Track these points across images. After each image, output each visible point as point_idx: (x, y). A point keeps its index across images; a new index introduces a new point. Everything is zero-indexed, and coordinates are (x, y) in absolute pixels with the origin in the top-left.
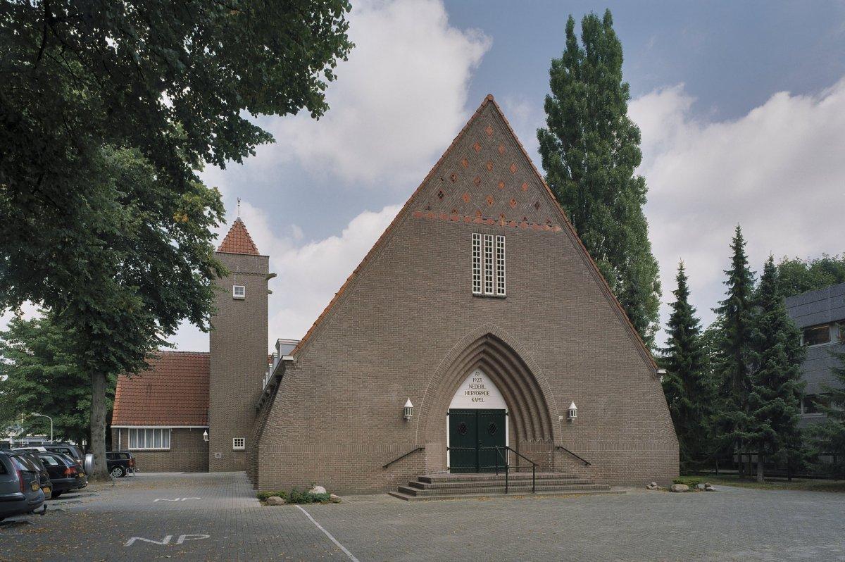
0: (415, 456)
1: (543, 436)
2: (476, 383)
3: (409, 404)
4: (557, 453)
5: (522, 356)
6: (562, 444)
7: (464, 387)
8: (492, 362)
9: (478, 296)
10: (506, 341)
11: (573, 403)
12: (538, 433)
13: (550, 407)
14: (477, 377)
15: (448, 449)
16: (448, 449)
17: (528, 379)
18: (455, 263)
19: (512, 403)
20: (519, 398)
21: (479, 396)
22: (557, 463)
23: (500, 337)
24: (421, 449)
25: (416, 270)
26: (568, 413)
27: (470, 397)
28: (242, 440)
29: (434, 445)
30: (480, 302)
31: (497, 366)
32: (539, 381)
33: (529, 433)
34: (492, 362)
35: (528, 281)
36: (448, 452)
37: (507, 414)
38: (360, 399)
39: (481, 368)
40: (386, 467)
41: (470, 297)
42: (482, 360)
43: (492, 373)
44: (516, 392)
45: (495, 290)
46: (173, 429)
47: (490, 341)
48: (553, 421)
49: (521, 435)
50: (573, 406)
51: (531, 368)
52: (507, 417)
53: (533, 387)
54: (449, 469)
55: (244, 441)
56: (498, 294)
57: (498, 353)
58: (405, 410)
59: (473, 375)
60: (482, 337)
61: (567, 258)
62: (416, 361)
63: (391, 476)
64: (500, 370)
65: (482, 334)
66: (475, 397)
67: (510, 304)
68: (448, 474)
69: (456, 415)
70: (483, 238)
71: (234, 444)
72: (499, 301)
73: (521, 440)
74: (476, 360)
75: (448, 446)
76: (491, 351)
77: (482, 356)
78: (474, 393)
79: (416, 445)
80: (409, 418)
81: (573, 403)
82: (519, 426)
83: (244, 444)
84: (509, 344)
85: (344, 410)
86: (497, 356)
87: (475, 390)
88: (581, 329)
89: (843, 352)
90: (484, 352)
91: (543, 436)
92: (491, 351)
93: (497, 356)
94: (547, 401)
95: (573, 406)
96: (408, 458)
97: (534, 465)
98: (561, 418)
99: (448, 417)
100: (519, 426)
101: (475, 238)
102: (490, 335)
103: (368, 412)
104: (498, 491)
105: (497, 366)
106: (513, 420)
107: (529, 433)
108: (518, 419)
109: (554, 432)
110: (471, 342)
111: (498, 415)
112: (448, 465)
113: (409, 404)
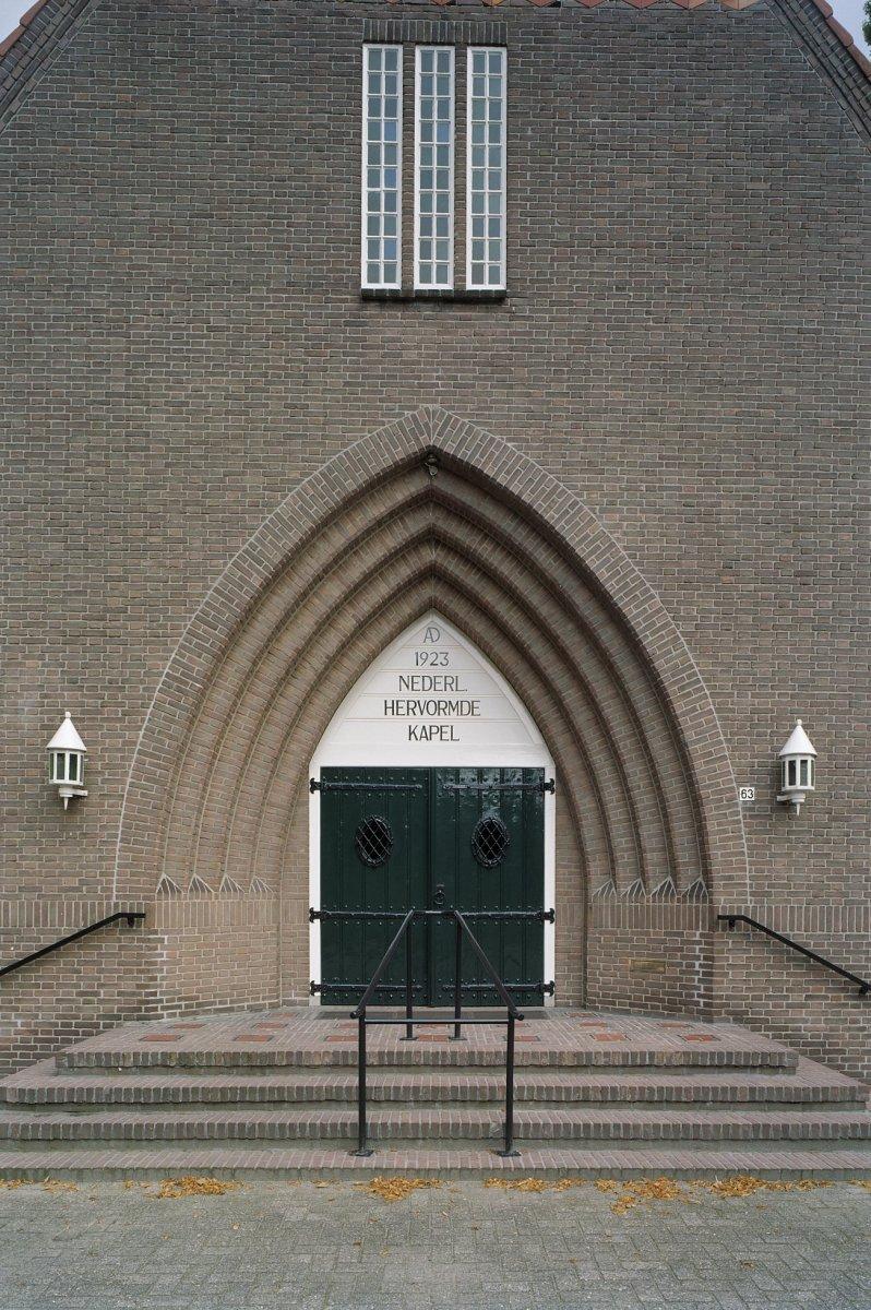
1: (672, 866)
4: (727, 942)
5: (571, 538)
6: (747, 905)
7: (383, 682)
8: (471, 580)
9: (380, 299)
10: (501, 480)
12: (653, 858)
13: (695, 749)
14: (429, 647)
15: (313, 915)
16: (313, 915)
17: (607, 636)
18: (286, 171)
19: (562, 741)
20: (582, 718)
21: (440, 720)
22: (723, 988)
23: (477, 461)
26: (778, 772)
27: (400, 725)
30: (391, 324)
31: (490, 596)
32: (649, 641)
33: (624, 858)
35: (604, 223)
41: (350, 304)
42: (432, 573)
44: (571, 696)
47: (447, 487)
48: (710, 811)
49: (596, 867)
50: (800, 743)
51: (611, 586)
52: (550, 801)
53: (627, 669)
54: (315, 988)
59: (417, 632)
64: (502, 608)
65: (400, 454)
66: (420, 721)
67: (518, 325)
69: (343, 788)
72: (474, 313)
73: (596, 888)
74: (404, 571)
75: (315, 903)
77: (430, 555)
78: (414, 707)
79: (116, 901)
80: (800, 799)
82: (590, 832)
84: (515, 488)
87: (423, 697)
88: (844, 417)
89: (1, 1081)
90: (432, 537)
91: (672, 866)
94: (685, 722)
95: (800, 743)
96: (76, 956)
98: (747, 794)
100: (590, 832)
102: (429, 460)
106: (568, 809)
107: (624, 858)
108: (585, 803)
109: (717, 855)
110: (351, 486)
111: (522, 790)
112: (316, 976)
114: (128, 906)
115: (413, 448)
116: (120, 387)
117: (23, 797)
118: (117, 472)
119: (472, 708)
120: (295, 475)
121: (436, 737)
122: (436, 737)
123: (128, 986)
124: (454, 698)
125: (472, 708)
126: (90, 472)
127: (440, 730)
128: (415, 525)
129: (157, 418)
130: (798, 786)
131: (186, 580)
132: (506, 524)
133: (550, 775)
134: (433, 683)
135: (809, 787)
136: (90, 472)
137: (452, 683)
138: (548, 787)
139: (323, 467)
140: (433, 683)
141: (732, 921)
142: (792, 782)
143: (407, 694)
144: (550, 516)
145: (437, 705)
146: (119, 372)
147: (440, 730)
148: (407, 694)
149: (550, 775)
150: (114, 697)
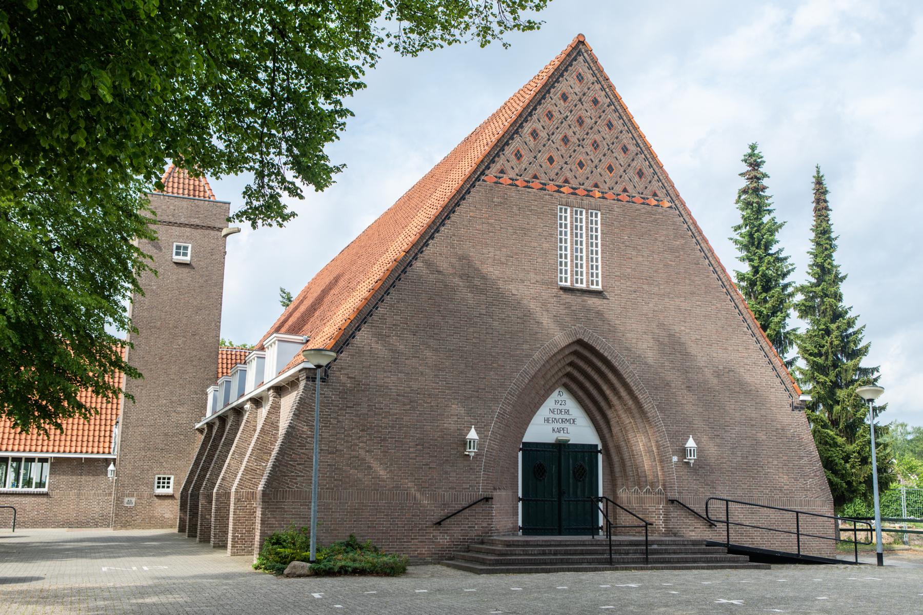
0: (478, 508)
2: (558, 406)
3: (473, 435)
5: (622, 372)
6: (676, 496)
7: (544, 412)
8: (581, 378)
10: (602, 351)
11: (473, 430)
14: (559, 398)
15: (520, 499)
16: (520, 499)
21: (563, 425)
23: (594, 345)
24: (487, 499)
25: (485, 251)
27: (549, 427)
28: (169, 479)
29: (503, 493)
34: (581, 378)
36: (520, 504)
37: (600, 452)
38: (407, 426)
39: (566, 386)
40: (439, 523)
43: (581, 393)
45: (587, 282)
46: (55, 458)
52: (600, 456)
55: (172, 481)
56: (592, 287)
57: (589, 366)
58: (464, 443)
59: (555, 395)
60: (570, 345)
61: (678, 243)
62: (482, 375)
63: (443, 539)
66: (557, 425)
68: (520, 537)
69: (531, 450)
70: (571, 212)
71: (156, 485)
75: (520, 495)
76: (581, 364)
77: (569, 369)
78: (555, 420)
79: (481, 493)
81: (473, 430)
83: (171, 485)
84: (606, 354)
85: (383, 440)
86: (589, 370)
87: (557, 417)
88: (698, 337)
92: (581, 364)
93: (589, 370)
97: (647, 524)
98: (675, 459)
99: (520, 454)
101: (561, 212)
102: (580, 342)
103: (417, 445)
104: (600, 562)
105: (588, 385)
111: (591, 450)
113: (473, 435)
114: (486, 494)
115: (574, 339)
116: (484, 312)
117: (458, 452)
118: (483, 341)
119: (574, 421)
120: (539, 346)
121: (562, 432)
122: (562, 432)
123: (485, 525)
124: (568, 417)
125: (574, 421)
126: (474, 340)
127: (563, 429)
128: (568, 360)
129: (496, 324)
130: (472, 450)
131: (505, 379)
132: (599, 364)
133: (600, 448)
134: (561, 411)
135: (476, 450)
136: (474, 340)
137: (567, 412)
138: (600, 452)
139: (547, 343)
140: (561, 411)
141: (672, 501)
142: (470, 448)
143: (552, 416)
144: (616, 364)
145: (562, 421)
146: (483, 307)
147: (563, 429)
148: (552, 416)
149: (600, 448)
150: (481, 419)
